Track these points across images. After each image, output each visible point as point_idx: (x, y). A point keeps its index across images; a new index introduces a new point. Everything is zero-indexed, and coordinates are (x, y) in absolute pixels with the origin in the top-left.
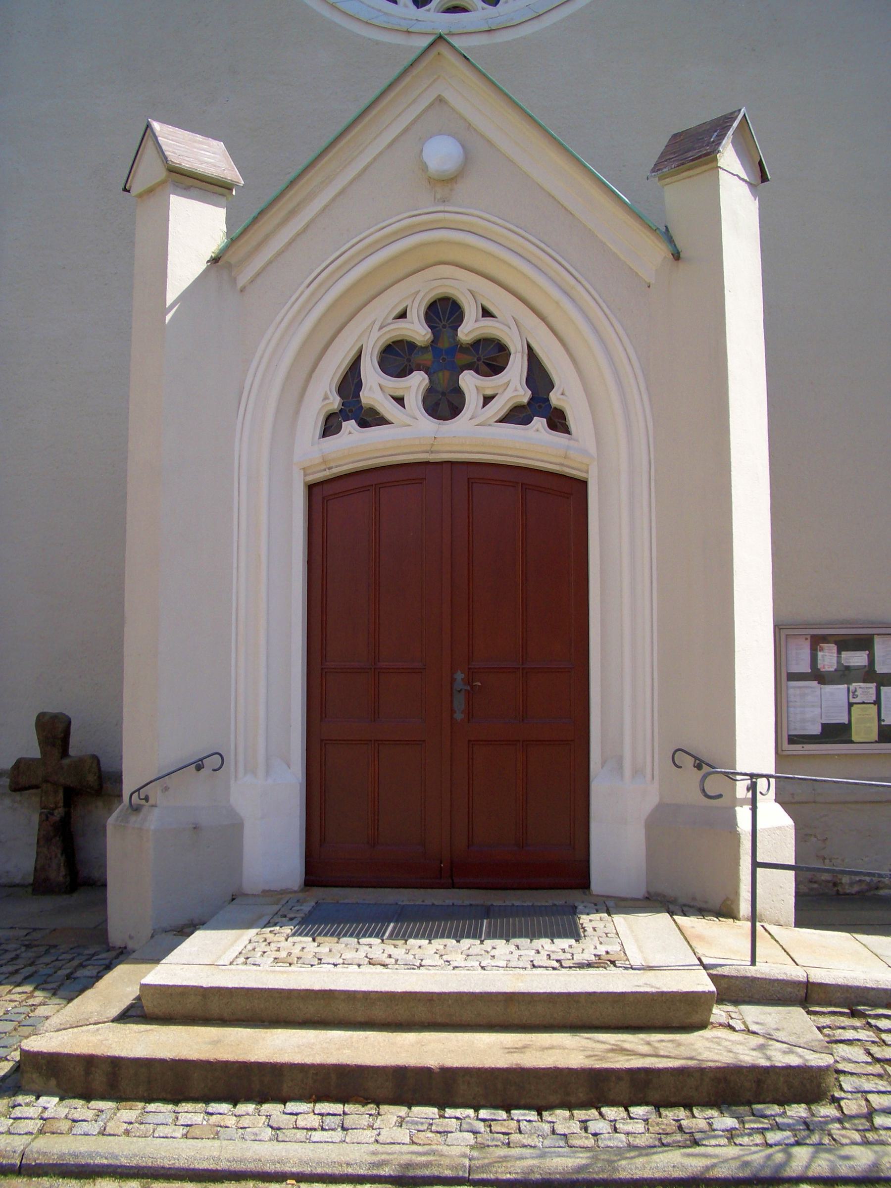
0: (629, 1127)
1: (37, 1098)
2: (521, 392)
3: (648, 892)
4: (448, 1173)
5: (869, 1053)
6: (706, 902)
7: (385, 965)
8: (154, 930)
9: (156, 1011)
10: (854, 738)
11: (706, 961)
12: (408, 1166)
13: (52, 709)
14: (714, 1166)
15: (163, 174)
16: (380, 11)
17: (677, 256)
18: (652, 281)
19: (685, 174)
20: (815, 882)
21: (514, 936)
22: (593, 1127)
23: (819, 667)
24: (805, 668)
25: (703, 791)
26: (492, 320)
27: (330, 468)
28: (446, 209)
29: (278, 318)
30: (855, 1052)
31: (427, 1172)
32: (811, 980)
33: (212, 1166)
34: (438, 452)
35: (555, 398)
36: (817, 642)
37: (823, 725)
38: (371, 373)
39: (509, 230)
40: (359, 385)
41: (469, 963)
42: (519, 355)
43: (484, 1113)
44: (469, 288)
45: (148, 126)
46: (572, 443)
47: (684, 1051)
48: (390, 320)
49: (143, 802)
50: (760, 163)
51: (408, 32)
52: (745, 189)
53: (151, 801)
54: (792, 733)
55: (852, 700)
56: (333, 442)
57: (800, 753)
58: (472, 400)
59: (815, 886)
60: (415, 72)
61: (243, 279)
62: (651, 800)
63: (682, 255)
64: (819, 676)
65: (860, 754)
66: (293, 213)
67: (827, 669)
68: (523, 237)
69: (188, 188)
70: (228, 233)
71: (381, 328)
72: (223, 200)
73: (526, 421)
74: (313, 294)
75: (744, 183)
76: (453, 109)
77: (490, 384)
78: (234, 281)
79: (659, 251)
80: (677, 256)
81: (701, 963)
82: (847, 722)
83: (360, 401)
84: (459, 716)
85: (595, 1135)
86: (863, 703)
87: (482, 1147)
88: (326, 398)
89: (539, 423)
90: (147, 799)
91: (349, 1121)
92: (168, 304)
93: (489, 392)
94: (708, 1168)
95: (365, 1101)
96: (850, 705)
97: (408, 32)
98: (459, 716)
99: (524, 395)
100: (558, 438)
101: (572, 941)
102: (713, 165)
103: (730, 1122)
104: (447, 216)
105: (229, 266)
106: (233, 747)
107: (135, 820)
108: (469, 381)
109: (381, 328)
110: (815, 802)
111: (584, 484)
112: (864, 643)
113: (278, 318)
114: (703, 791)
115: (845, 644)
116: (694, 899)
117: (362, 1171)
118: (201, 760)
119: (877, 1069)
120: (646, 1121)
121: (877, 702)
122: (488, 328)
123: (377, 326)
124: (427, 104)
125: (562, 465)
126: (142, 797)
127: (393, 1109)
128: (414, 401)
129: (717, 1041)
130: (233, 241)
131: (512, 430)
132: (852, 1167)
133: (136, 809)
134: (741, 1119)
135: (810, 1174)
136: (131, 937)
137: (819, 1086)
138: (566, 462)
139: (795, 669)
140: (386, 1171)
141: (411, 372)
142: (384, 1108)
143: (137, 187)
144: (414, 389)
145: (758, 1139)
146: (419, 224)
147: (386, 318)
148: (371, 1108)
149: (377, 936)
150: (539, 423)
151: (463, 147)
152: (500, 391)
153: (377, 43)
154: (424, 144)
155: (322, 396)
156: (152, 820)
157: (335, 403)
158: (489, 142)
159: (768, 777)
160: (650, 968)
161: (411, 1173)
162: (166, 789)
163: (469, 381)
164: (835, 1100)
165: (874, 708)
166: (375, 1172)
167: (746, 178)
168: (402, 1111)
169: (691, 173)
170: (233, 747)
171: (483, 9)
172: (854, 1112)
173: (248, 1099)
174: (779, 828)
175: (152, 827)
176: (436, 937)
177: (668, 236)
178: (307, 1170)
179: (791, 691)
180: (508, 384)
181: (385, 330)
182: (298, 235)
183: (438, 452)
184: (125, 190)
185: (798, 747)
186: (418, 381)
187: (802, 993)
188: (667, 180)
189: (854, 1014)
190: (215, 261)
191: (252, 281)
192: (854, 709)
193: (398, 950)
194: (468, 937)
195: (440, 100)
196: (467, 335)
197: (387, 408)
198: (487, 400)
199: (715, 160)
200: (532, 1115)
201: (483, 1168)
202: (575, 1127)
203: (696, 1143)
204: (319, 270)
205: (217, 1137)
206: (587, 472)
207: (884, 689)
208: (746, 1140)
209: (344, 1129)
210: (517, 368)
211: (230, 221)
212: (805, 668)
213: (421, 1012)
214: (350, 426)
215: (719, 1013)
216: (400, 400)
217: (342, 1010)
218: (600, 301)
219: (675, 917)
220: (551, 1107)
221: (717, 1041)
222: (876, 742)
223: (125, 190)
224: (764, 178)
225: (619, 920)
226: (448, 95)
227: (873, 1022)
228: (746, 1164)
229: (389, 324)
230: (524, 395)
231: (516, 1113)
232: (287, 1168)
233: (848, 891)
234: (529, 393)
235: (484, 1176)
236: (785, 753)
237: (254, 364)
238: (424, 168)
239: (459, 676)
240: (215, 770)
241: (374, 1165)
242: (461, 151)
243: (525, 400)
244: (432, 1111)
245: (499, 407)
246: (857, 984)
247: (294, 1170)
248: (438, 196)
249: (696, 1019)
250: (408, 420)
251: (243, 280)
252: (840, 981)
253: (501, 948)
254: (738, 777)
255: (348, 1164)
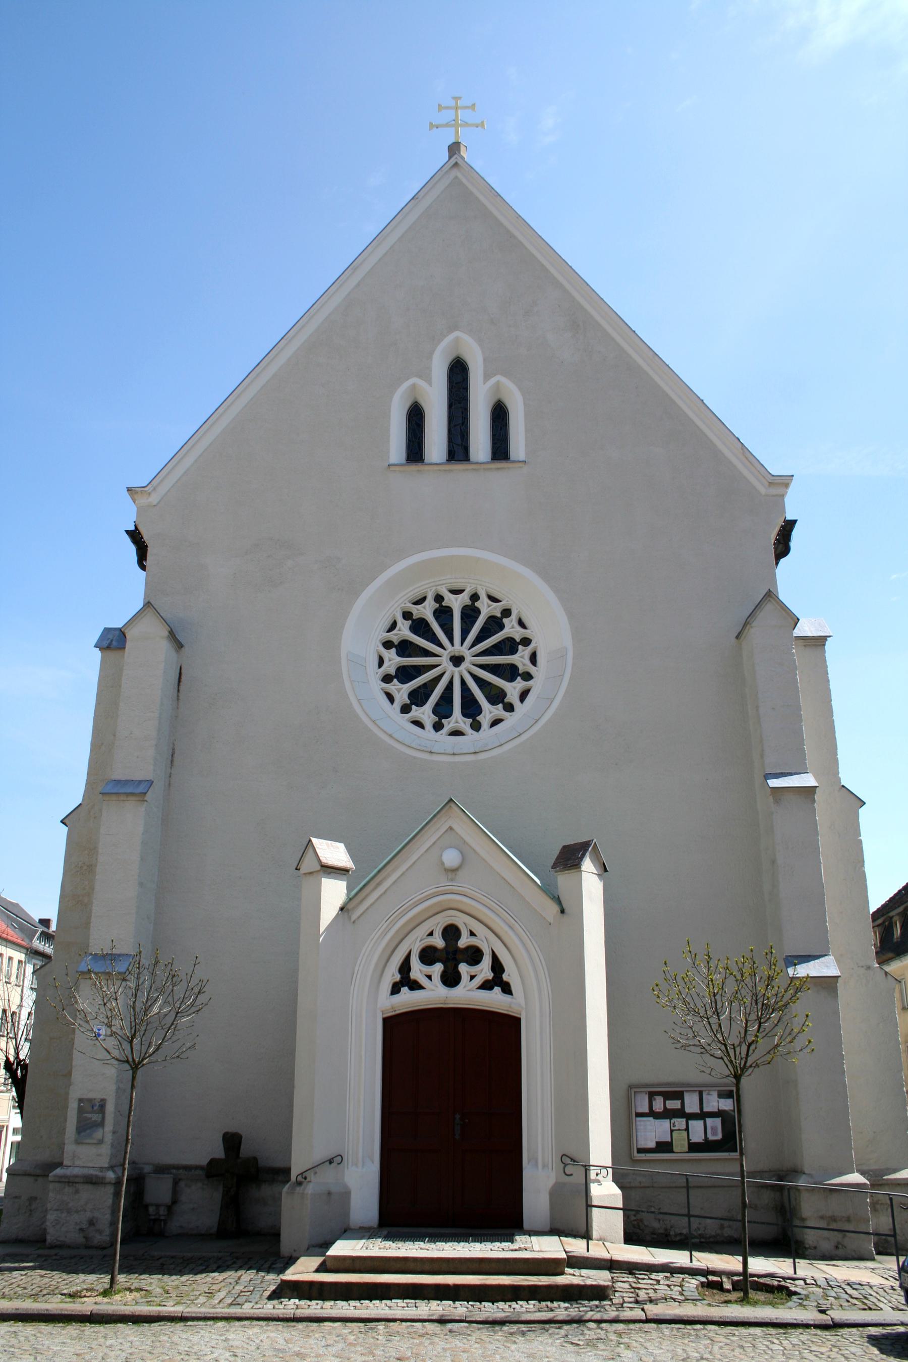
0: (528, 1306)
1: (289, 1300)
2: (489, 974)
3: (551, 1228)
4: (457, 1318)
5: (631, 1285)
6: (578, 1232)
7: (428, 1250)
8: (309, 1245)
9: (332, 1267)
10: (675, 1149)
11: (566, 1250)
12: (442, 1316)
13: (232, 1129)
14: (557, 1316)
15: (319, 868)
16: (415, 735)
17: (563, 911)
18: (552, 921)
19: (567, 872)
20: (655, 1234)
21: (484, 1241)
22: (513, 1306)
23: (654, 1109)
24: (646, 1110)
25: (565, 1172)
26: (465, 470)
27: (395, 1011)
28: (453, 884)
29: (372, 937)
30: (626, 1286)
31: (449, 1318)
32: (613, 1259)
33: (368, 1317)
34: (448, 1004)
35: (505, 977)
36: (652, 1095)
37: (657, 1143)
38: (415, 963)
39: (484, 895)
40: (409, 969)
41: (464, 1249)
42: (488, 956)
43: (470, 1303)
44: (465, 922)
45: (310, 841)
46: (514, 1000)
47: (551, 1280)
48: (425, 936)
49: (303, 1180)
50: (604, 864)
51: (431, 752)
52: (596, 878)
53: (308, 1179)
54: (639, 1147)
55: (673, 1128)
56: (397, 998)
57: (644, 1158)
58: (465, 978)
59: (655, 1236)
60: (438, 816)
61: (354, 917)
62: (551, 1182)
63: (565, 911)
64: (652, 1114)
65: (666, 1160)
66: (379, 884)
67: (658, 1110)
68: (489, 898)
69: (329, 873)
70: (348, 894)
71: (421, 941)
72: (345, 877)
73: (491, 988)
74: (389, 925)
75: (594, 875)
76: (457, 833)
77: (474, 970)
78: (350, 918)
79: (555, 908)
80: (563, 911)
81: (565, 1250)
82: (670, 1140)
83: (409, 977)
84: (457, 1137)
85: (514, 1309)
86: (679, 1130)
87: (470, 1311)
88: (393, 975)
89: (497, 989)
90: (305, 1178)
91: (417, 1305)
92: (321, 933)
93: (473, 974)
94: (555, 1317)
95: (423, 1299)
96: (672, 1131)
97: (431, 752)
98: (457, 1137)
99: (490, 976)
100: (506, 998)
101: (510, 1243)
102: (579, 870)
103: (567, 1305)
104: (454, 887)
105: (348, 910)
106: (346, 1153)
107: (299, 1189)
108: (463, 968)
109: (421, 941)
110: (653, 1187)
111: (517, 1021)
112: (679, 1096)
113: (372, 937)
114: (565, 1172)
115: (667, 1096)
116: (572, 1231)
117: (425, 1318)
118: (333, 1159)
119: (633, 1290)
120: (534, 1305)
121: (687, 1129)
122: (473, 941)
123: (419, 939)
124: (445, 830)
125: (507, 1011)
126: (303, 1177)
127: (434, 1301)
128: (437, 978)
129: (567, 1278)
130: (350, 900)
131: (484, 993)
132: (609, 1317)
133: (299, 1184)
134: (572, 1305)
135: (593, 1318)
136: (295, 1251)
137: (604, 1294)
138: (510, 1010)
139: (640, 1110)
140: (434, 1317)
141: (434, 963)
142: (431, 1301)
143: (304, 868)
144: (437, 972)
145: (576, 1309)
146: (440, 891)
147: (423, 936)
148: (426, 1301)
149: (422, 1241)
150: (497, 989)
151: (462, 853)
152: (478, 973)
153: (415, 758)
154: (443, 852)
155: (391, 975)
156: (310, 1189)
157: (398, 977)
158: (474, 850)
159: (606, 1167)
160: (541, 1251)
161: (443, 1318)
162: (316, 1173)
163: (463, 968)
164: (611, 1300)
165: (685, 1133)
166: (430, 1318)
167: (596, 872)
168: (439, 1302)
169: (569, 871)
170: (346, 1153)
171: (472, 734)
172: (617, 1303)
173: (376, 1299)
174: (613, 1195)
175: (310, 1192)
176: (448, 1242)
177: (558, 901)
178: (405, 1317)
179: (638, 1123)
180: (482, 970)
181: (423, 942)
182: (381, 895)
183: (448, 1004)
184: (296, 869)
185: (643, 1155)
186: (438, 968)
187: (609, 1264)
188: (559, 873)
189: (631, 1273)
190: (342, 909)
191: (359, 918)
192: (674, 1134)
193: (433, 1246)
194: (463, 1242)
195: (451, 828)
196: (462, 945)
197: (423, 981)
198: (472, 977)
199: (580, 867)
200: (490, 1304)
201: (470, 1316)
202: (507, 1306)
203: (552, 1311)
204: (391, 914)
205: (367, 1309)
206: (520, 1015)
207: (690, 1122)
208: (572, 1310)
209: (416, 1307)
210: (487, 962)
211: (349, 888)
212: (646, 1110)
213: (444, 1267)
214: (405, 989)
215: (567, 1270)
216: (429, 977)
217: (411, 1266)
218: (526, 931)
219: (561, 1238)
220: (497, 1301)
221: (567, 1278)
222: (687, 1152)
223: (296, 869)
224: (606, 870)
225: (534, 1238)
226: (455, 826)
227: (637, 1276)
228: (569, 1315)
229: (424, 939)
230: (490, 976)
231: (483, 1303)
232: (397, 1317)
233: (674, 1240)
234: (492, 975)
235: (471, 1319)
236: (636, 1158)
237: (360, 958)
238: (443, 864)
239: (458, 1116)
240: (338, 1164)
241: (429, 1315)
242: (460, 855)
243: (491, 978)
244: (451, 1302)
245: (478, 981)
246: (633, 1261)
247: (400, 1317)
248: (449, 878)
249: (559, 1270)
250: (434, 988)
251: (354, 917)
252: (626, 1259)
253: (478, 1245)
254: (592, 1168)
255: (420, 1315)
